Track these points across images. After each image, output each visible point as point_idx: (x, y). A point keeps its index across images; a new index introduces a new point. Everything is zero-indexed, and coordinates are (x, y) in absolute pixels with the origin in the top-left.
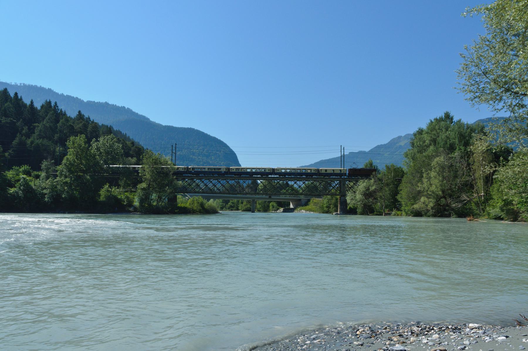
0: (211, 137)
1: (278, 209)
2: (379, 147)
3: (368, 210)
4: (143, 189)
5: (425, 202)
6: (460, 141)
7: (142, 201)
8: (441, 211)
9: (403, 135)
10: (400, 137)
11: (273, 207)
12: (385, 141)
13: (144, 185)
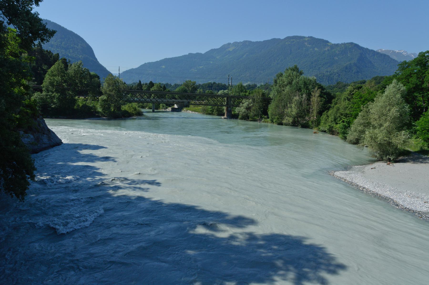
0: (68, 30)
1: (167, 108)
2: (212, 51)
3: (246, 118)
4: (104, 101)
5: (288, 120)
6: (304, 87)
7: (104, 108)
8: (294, 124)
9: (232, 42)
10: (229, 44)
11: (163, 106)
12: (217, 46)
13: (104, 97)
